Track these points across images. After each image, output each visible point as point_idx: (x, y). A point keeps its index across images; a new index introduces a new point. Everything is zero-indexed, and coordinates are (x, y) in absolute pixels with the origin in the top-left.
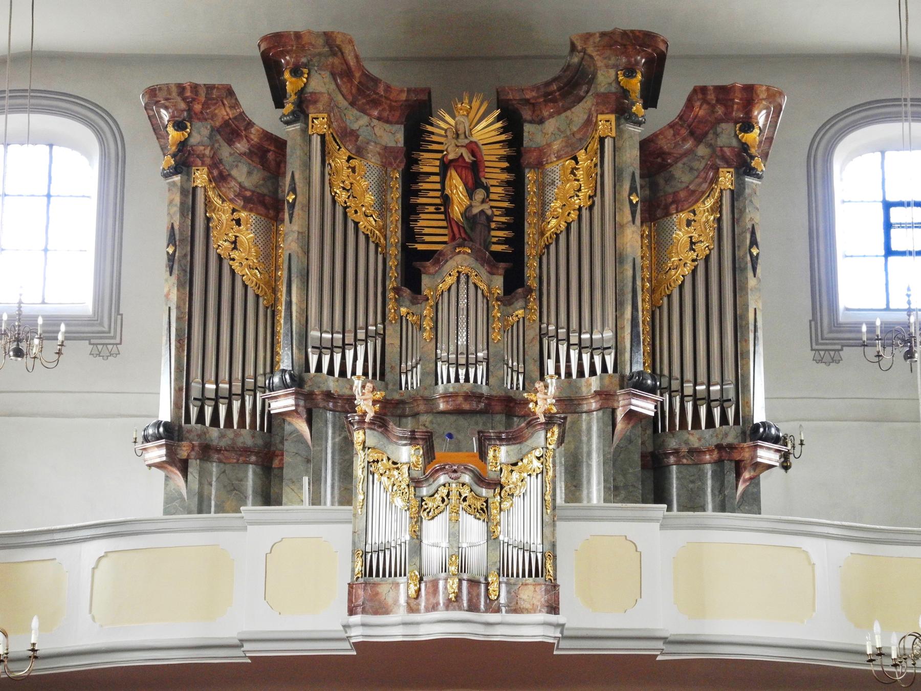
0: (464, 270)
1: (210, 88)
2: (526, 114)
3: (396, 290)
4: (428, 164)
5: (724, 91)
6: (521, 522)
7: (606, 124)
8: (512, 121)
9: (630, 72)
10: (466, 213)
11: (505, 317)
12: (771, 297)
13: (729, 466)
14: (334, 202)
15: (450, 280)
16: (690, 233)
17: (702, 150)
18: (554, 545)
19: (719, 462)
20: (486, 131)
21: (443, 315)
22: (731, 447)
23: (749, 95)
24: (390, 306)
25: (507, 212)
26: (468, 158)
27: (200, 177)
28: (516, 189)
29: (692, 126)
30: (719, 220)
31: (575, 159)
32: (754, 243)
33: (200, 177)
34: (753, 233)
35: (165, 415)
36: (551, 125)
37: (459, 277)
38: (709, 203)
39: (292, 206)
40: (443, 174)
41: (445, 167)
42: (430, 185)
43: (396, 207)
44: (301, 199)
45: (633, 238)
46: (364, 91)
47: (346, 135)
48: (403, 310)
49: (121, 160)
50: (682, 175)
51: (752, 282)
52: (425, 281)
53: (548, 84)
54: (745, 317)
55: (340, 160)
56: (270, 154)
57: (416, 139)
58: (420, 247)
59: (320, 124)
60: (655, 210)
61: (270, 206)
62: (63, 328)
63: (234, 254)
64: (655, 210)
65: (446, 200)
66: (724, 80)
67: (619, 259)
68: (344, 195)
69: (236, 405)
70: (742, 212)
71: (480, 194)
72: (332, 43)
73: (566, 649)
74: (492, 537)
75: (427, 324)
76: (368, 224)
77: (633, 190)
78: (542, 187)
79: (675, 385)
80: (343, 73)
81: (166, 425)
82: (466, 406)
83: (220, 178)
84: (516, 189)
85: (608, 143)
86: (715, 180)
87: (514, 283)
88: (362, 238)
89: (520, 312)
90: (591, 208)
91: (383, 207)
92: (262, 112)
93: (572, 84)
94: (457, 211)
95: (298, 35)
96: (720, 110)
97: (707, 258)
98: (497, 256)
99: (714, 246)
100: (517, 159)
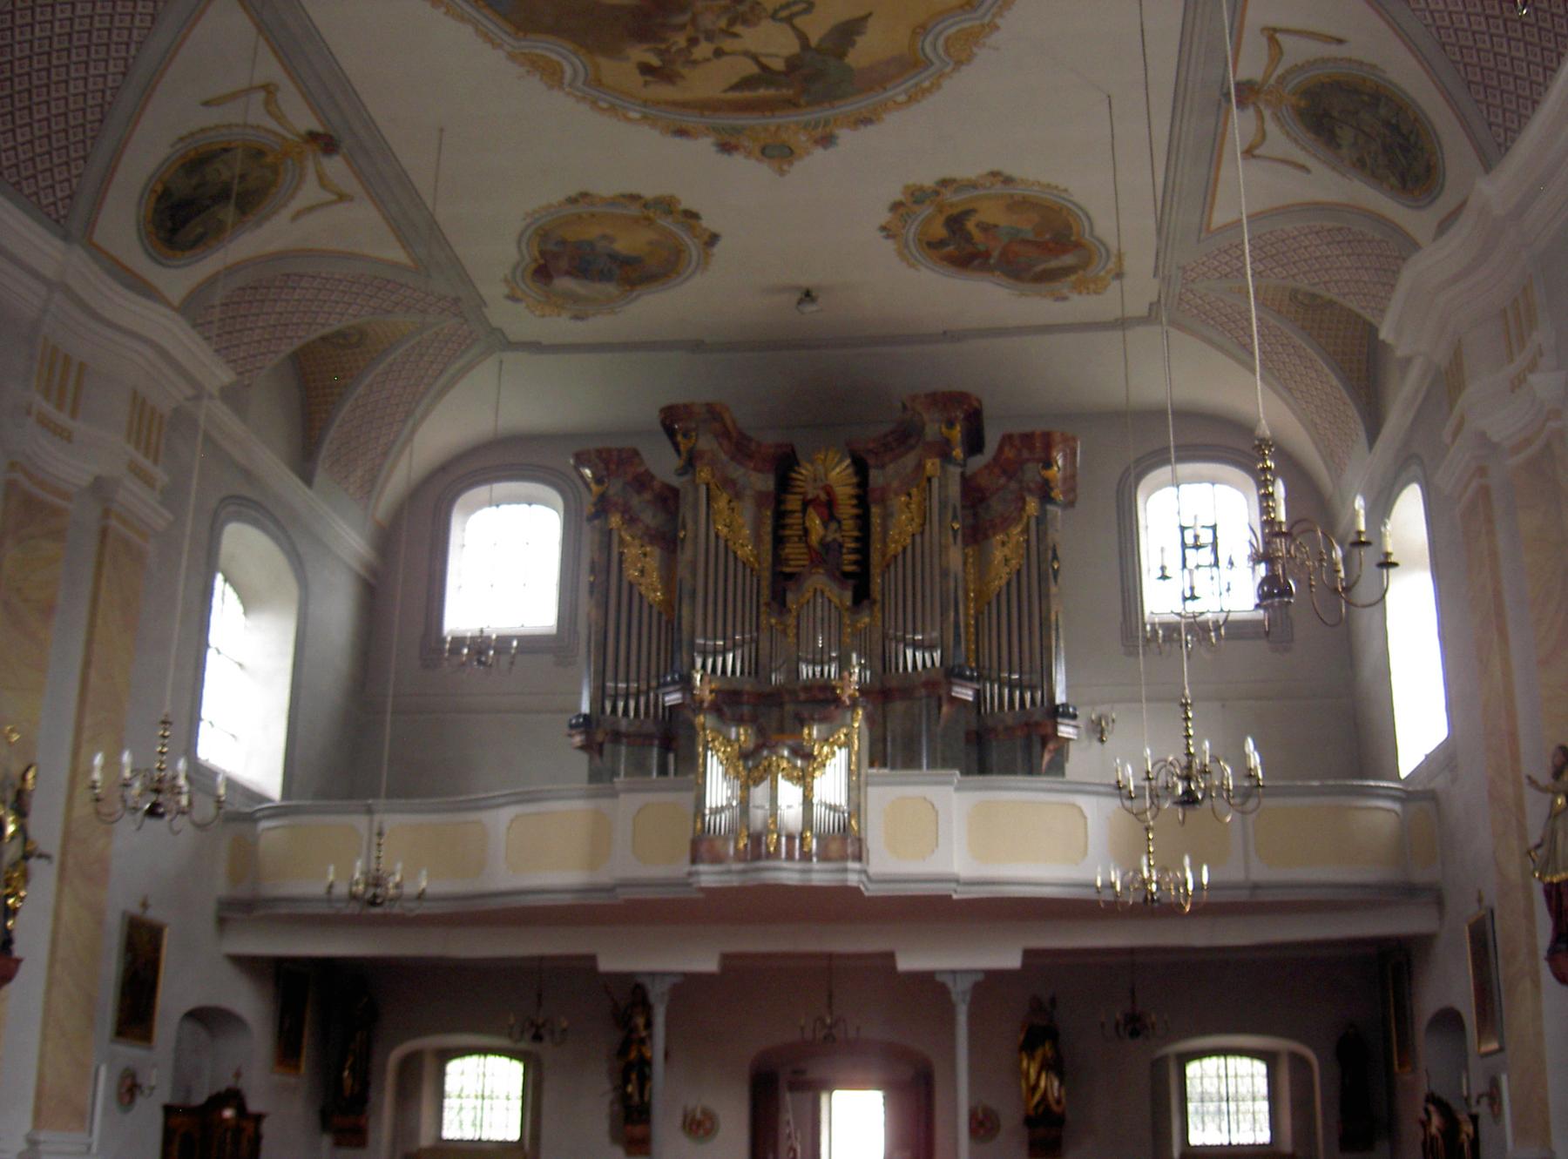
0: (819, 587)
1: (620, 451)
2: (871, 461)
3: (768, 605)
4: (793, 503)
5: (1027, 438)
6: (831, 784)
7: (932, 465)
8: (861, 468)
9: (951, 424)
10: (822, 542)
11: (853, 625)
12: (1074, 601)
13: (1036, 740)
14: (717, 536)
15: (809, 595)
16: (1004, 551)
17: (1013, 485)
18: (859, 805)
19: (1028, 737)
20: (840, 475)
21: (803, 624)
22: (1037, 724)
23: (1047, 441)
24: (763, 617)
25: (857, 539)
26: (823, 497)
27: (615, 520)
28: (863, 521)
29: (1007, 468)
30: (1027, 541)
31: (909, 495)
32: (1055, 557)
33: (615, 520)
34: (1054, 551)
35: (585, 708)
36: (891, 468)
37: (822, 592)
38: (1019, 529)
39: (683, 540)
40: (804, 511)
41: (806, 504)
42: (794, 520)
43: (768, 539)
44: (690, 535)
45: (955, 556)
46: (741, 447)
47: (728, 483)
48: (773, 621)
49: (258, 506)
50: (996, 506)
51: (1054, 589)
52: (790, 597)
53: (886, 436)
54: (1048, 619)
55: (722, 503)
56: (668, 499)
57: (784, 484)
58: (788, 570)
59: (704, 474)
60: (976, 535)
61: (668, 541)
62: (515, 643)
63: (642, 580)
64: (976, 535)
65: (806, 532)
66: (1027, 429)
67: (945, 573)
68: (725, 530)
69: (642, 700)
70: (1045, 533)
71: (833, 526)
72: (713, 413)
73: (871, 890)
74: (807, 802)
75: (791, 632)
76: (746, 551)
77: (955, 518)
78: (886, 517)
79: (994, 675)
80: (724, 434)
81: (585, 716)
82: (821, 696)
83: (631, 520)
84: (863, 521)
85: (935, 483)
86: (1023, 509)
87: (862, 595)
88: (740, 565)
89: (867, 620)
90: (922, 533)
91: (757, 538)
92: (663, 463)
93: (905, 436)
94: (814, 539)
95: (686, 406)
96: (1025, 454)
97: (1019, 572)
98: (846, 575)
99: (1023, 562)
100: (863, 498)
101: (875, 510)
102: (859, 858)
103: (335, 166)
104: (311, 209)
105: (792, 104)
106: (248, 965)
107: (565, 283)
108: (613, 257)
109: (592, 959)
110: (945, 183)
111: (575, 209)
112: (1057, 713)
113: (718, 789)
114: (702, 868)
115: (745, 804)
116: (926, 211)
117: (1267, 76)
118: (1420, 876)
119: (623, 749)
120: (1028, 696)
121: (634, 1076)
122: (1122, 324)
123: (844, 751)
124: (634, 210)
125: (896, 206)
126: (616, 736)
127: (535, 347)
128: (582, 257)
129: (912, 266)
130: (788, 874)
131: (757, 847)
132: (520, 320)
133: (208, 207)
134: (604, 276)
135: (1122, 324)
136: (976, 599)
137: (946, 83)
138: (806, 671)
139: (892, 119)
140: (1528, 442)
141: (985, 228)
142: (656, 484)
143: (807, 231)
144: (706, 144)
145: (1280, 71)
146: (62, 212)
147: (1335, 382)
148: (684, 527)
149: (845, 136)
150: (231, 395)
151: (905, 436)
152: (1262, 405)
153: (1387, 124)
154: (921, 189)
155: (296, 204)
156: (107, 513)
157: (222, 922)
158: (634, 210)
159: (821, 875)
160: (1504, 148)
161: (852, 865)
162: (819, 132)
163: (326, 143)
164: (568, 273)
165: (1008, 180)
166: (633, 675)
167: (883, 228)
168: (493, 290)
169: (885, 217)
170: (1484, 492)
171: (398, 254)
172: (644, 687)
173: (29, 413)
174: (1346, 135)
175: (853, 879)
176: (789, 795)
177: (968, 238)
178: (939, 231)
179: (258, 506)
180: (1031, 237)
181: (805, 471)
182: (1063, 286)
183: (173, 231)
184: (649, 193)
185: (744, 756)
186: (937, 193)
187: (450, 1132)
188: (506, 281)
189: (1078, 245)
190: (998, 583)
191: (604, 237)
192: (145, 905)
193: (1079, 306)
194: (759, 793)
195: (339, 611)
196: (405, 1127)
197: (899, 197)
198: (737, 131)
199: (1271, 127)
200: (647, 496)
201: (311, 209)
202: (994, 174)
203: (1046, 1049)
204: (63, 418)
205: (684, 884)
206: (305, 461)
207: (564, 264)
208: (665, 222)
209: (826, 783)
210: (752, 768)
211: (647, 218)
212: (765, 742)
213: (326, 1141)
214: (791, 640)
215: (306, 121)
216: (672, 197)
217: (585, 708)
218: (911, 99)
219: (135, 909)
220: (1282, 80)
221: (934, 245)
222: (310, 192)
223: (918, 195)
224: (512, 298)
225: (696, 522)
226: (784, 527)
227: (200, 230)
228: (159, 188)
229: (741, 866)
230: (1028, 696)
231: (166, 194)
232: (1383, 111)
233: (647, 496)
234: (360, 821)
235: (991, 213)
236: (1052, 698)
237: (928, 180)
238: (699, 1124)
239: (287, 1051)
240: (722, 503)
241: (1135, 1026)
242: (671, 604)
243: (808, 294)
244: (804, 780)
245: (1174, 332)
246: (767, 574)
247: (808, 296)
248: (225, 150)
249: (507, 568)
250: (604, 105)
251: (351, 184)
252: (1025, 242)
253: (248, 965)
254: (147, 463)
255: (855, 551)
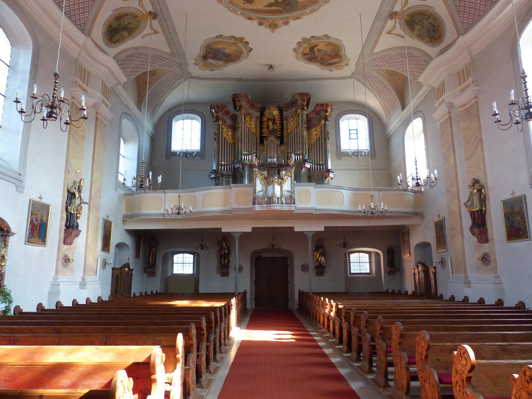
2: (284, 110)
4: (265, 119)
5: (322, 105)
6: (287, 186)
7: (299, 111)
8: (281, 111)
11: (280, 149)
16: (315, 132)
17: (318, 117)
20: (276, 113)
24: (258, 147)
25: (280, 129)
27: (221, 122)
32: (328, 134)
33: (221, 122)
35: (214, 168)
36: (289, 111)
37: (272, 141)
40: (268, 121)
41: (268, 120)
42: (265, 123)
45: (305, 133)
47: (249, 114)
49: (129, 115)
51: (328, 142)
52: (265, 142)
56: (234, 118)
57: (262, 115)
60: (309, 128)
61: (234, 128)
64: (309, 128)
65: (268, 126)
71: (275, 125)
83: (224, 123)
86: (320, 122)
87: (282, 142)
91: (256, 128)
94: (270, 128)
100: (282, 119)
101: (285, 121)
102: (294, 204)
103: (155, 23)
104: (147, 35)
105: (280, 12)
106: (131, 232)
107: (210, 61)
108: (224, 54)
109: (220, 229)
110: (312, 37)
111: (219, 40)
112: (329, 171)
113: (259, 187)
114: (256, 206)
115: (266, 190)
116: (306, 45)
117: (400, 11)
118: (418, 211)
119: (224, 178)
120: (321, 167)
121: (223, 258)
122: (344, 78)
123: (289, 178)
124: (232, 41)
125: (299, 43)
126: (222, 175)
127: (199, 78)
128: (215, 53)
129: (298, 60)
130: (277, 207)
131: (270, 201)
132: (195, 70)
133: (120, 31)
134: (220, 59)
135: (344, 78)
136: (308, 144)
137: (321, 8)
138: (269, 160)
139: (305, 18)
140: (465, 105)
141: (319, 50)
142: (231, 114)
143: (274, 50)
144: (255, 22)
145: (405, 9)
146: (82, 27)
147: (394, 94)
148: (239, 124)
149: (292, 22)
150: (124, 86)
151: (293, 103)
152: (373, 102)
153: (431, 24)
154: (306, 39)
155: (143, 33)
156: (97, 113)
157: (124, 221)
158: (232, 41)
159: (286, 208)
160: (467, 30)
161: (293, 205)
162: (285, 21)
163: (154, 15)
164: (212, 58)
165: (328, 37)
166: (226, 160)
167: (294, 49)
168: (191, 61)
169: (295, 46)
170: (450, 117)
171: (168, 50)
172: (228, 163)
173: (76, 83)
174: (417, 27)
175: (293, 209)
176: (277, 188)
177: (314, 53)
178: (307, 51)
179: (129, 115)
180: (329, 53)
181: (267, 112)
182: (332, 68)
183: (112, 37)
184: (237, 36)
185: (266, 178)
186: (310, 40)
187: (175, 272)
188: (195, 59)
189: (340, 56)
190: (313, 141)
191: (223, 48)
192: (108, 217)
193: (336, 73)
194: (270, 188)
195: (146, 143)
196: (164, 272)
197: (300, 41)
198: (264, 19)
199: (397, 25)
200: (228, 116)
201: (147, 35)
202: (325, 35)
203: (321, 250)
204: (84, 86)
205: (251, 209)
206: (139, 104)
207: (211, 55)
208: (240, 45)
209: (283, 187)
210: (268, 181)
211: (235, 43)
212: (270, 175)
213: (145, 275)
214: (265, 152)
215: (149, 8)
216: (243, 37)
217: (214, 168)
218: (311, 12)
219: (106, 218)
220: (404, 12)
221: (305, 55)
222: (148, 30)
223: (305, 40)
224: (196, 64)
225: (242, 123)
226: (262, 125)
227: (118, 38)
228: (109, 24)
229: (266, 205)
230: (321, 167)
231: (110, 26)
232: (431, 20)
233: (228, 116)
234: (162, 195)
235: (322, 47)
236: (328, 168)
237: (308, 36)
238: (305, 268)
239: (137, 254)
240: (248, 119)
241: (345, 245)
242: (234, 143)
243: (271, 66)
244: (280, 184)
245: (355, 81)
246: (259, 136)
247: (271, 67)
248: (127, 15)
249: (187, 134)
250: (231, 9)
251: (159, 29)
252: (327, 55)
253: (131, 232)
254: (106, 100)
255: (280, 131)
